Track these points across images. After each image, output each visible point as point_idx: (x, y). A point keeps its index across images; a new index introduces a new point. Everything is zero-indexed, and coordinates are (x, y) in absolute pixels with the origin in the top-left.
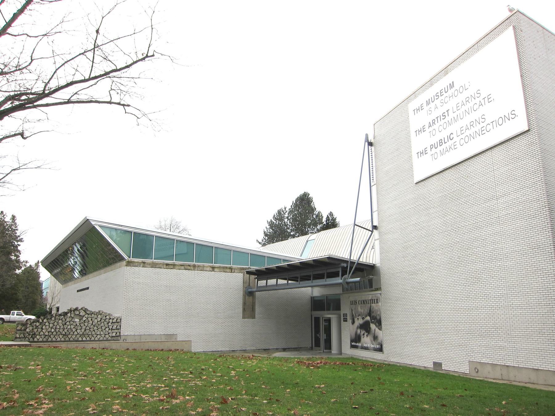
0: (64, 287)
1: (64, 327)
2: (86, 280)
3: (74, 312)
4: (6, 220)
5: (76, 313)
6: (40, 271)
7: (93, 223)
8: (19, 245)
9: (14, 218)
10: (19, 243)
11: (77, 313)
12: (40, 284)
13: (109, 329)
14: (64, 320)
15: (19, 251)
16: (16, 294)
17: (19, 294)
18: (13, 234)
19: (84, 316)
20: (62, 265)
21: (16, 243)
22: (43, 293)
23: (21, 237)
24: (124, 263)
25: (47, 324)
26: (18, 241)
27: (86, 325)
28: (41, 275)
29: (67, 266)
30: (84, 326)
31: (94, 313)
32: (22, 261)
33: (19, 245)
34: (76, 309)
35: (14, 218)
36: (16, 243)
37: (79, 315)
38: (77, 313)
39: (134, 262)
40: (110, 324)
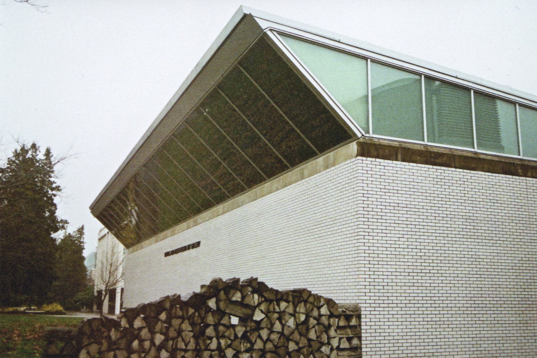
0: (133, 252)
1: (197, 344)
2: (188, 228)
3: (227, 294)
4: (38, 158)
5: (234, 299)
6: (85, 241)
7: (263, 25)
8: (55, 195)
9: (48, 153)
10: (54, 192)
11: (237, 297)
12: (83, 259)
13: (332, 350)
14: (197, 319)
15: (55, 205)
16: (51, 269)
17: (56, 269)
18: (47, 178)
19: (255, 307)
20: (119, 224)
21: (50, 192)
22: (87, 271)
23: (57, 184)
24: (353, 147)
25: (145, 333)
26: (53, 189)
27: (265, 337)
28: (86, 246)
29: (127, 225)
30: (259, 341)
31: (285, 298)
32: (59, 220)
33: (55, 195)
34: (234, 284)
35: (48, 153)
36: (50, 192)
37: (242, 304)
38: (237, 297)
39: (283, 188)
40: (332, 333)
